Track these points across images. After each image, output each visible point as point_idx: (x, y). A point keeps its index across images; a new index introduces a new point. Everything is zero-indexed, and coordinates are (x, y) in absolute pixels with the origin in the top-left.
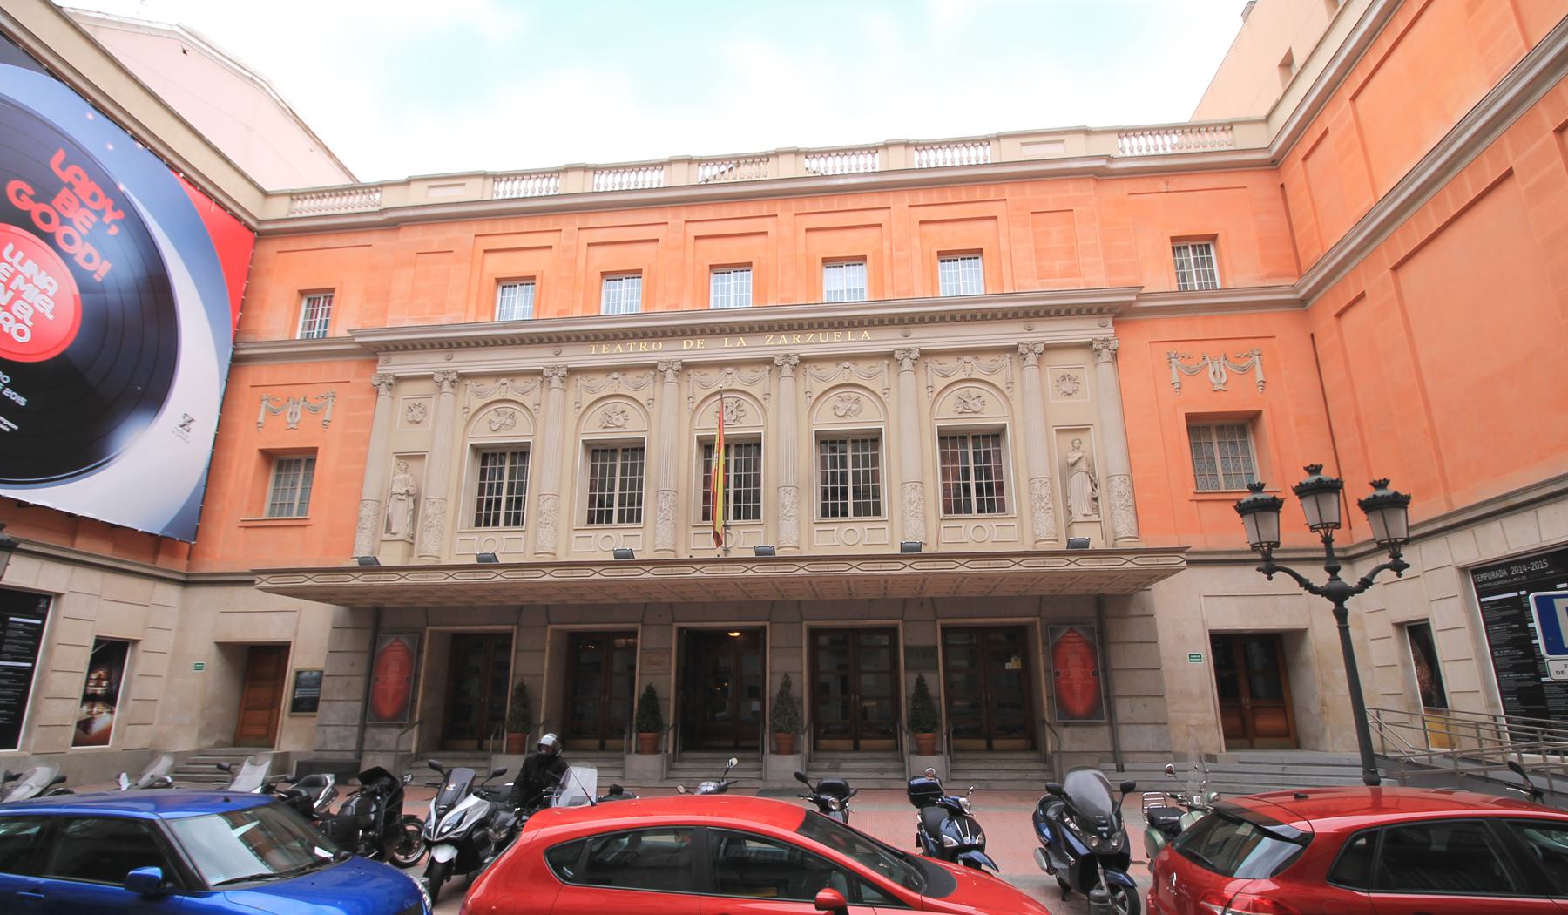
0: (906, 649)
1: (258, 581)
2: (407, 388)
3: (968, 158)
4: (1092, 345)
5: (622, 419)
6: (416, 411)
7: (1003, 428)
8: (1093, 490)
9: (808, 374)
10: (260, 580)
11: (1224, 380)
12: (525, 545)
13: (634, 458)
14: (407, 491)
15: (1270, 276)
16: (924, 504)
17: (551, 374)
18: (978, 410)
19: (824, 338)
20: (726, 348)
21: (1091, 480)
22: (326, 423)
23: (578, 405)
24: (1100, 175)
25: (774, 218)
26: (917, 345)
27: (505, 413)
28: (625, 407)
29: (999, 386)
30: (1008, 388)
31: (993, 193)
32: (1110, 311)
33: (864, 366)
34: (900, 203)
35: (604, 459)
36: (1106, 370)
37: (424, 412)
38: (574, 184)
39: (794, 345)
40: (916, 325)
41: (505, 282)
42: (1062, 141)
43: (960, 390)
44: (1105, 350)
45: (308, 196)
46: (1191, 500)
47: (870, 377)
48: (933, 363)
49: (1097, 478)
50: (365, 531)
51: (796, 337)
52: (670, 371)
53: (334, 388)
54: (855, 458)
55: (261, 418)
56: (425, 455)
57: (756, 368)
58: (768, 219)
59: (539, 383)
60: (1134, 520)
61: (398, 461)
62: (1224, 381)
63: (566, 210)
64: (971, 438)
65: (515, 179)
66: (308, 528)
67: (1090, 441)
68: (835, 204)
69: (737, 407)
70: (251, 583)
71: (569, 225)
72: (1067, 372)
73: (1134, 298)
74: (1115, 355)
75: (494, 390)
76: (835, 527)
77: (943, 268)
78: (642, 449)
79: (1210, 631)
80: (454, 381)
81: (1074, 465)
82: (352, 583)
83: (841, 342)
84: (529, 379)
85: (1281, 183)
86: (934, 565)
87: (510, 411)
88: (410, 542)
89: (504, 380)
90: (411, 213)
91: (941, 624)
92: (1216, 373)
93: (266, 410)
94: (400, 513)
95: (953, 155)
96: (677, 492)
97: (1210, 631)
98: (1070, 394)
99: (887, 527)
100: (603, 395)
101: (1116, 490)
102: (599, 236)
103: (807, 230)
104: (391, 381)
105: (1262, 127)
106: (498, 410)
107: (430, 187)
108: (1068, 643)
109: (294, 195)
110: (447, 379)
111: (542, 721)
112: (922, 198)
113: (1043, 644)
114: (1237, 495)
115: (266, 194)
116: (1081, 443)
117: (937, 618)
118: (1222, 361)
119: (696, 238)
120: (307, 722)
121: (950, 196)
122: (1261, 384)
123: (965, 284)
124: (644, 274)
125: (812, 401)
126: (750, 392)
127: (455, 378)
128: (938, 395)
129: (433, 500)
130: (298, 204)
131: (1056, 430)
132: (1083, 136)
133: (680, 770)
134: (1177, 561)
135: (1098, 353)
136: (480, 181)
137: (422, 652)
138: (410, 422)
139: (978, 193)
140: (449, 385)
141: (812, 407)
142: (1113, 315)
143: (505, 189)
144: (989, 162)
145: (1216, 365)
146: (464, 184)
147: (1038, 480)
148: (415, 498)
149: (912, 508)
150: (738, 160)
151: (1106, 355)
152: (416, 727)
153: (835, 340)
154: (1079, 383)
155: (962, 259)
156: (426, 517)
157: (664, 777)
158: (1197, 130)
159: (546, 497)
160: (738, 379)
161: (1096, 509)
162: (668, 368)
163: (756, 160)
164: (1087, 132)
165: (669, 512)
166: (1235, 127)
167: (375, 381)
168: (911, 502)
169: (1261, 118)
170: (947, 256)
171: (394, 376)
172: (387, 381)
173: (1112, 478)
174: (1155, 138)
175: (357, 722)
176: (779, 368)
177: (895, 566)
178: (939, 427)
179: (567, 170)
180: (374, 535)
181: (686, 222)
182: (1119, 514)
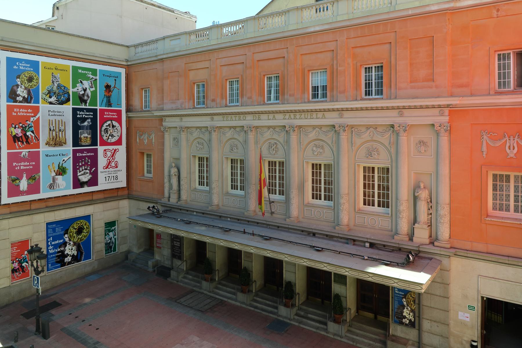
103: (301, 55)
119: (258, 61)
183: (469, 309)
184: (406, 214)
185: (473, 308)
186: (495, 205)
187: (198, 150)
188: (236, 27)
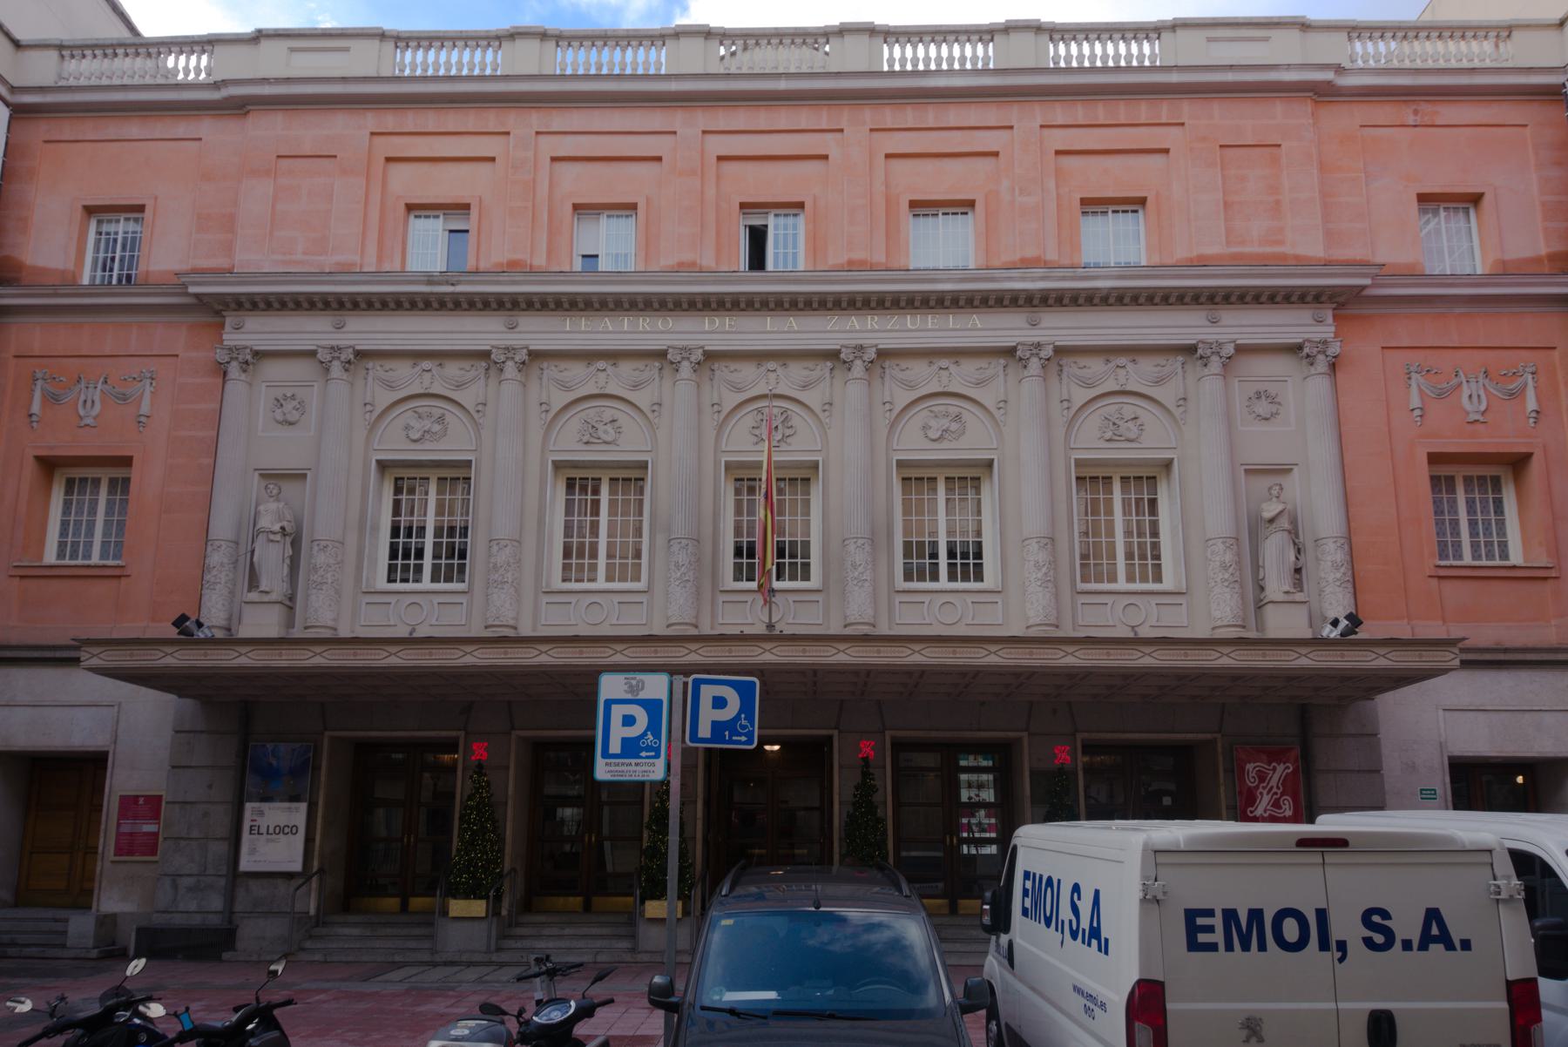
0: (1032, 773)
1: (83, 655)
2: (274, 370)
3: (572, 64)
4: (1196, 351)
5: (1135, 429)
6: (289, 406)
8: (1297, 558)
9: (887, 377)
10: (88, 656)
11: (1483, 408)
14: (283, 528)
16: (1055, 569)
17: (503, 358)
20: (728, 332)
21: (1295, 544)
22: (142, 419)
23: (544, 407)
24: (1322, 93)
25: (838, 135)
26: (702, 343)
27: (430, 415)
28: (618, 415)
30: (824, 411)
31: (1164, 111)
32: (1331, 298)
33: (969, 367)
34: (1027, 119)
35: (1139, 491)
36: (1317, 386)
37: (301, 407)
38: (525, 60)
39: (641, 332)
43: (1110, 407)
44: (1321, 357)
45: (88, 52)
47: (979, 383)
49: (1301, 540)
50: (218, 587)
52: (858, 362)
55: (36, 408)
56: (1291, 469)
57: (810, 364)
58: (829, 136)
59: (657, 371)
60: (1353, 601)
61: (263, 483)
64: (1461, 479)
65: (430, 46)
66: (123, 581)
67: (1293, 486)
68: (931, 116)
69: (782, 422)
70: (75, 661)
71: (524, 123)
72: (1261, 387)
73: (1368, 281)
74: (1333, 367)
75: (409, 377)
79: (1450, 758)
80: (349, 362)
81: (1271, 521)
82: (1297, 662)
84: (466, 364)
87: (437, 412)
88: (289, 603)
89: (426, 364)
91: (1083, 740)
92: (1472, 398)
93: (43, 396)
94: (272, 559)
96: (698, 541)
98: (1266, 419)
101: (1329, 558)
102: (568, 146)
103: (888, 156)
104: (249, 357)
106: (933, 409)
107: (292, 50)
109: (63, 49)
111: (315, 870)
112: (1059, 114)
113: (1226, 771)
114: (1541, 571)
115: (17, 44)
116: (1282, 489)
118: (1481, 380)
119: (720, 158)
121: (1101, 112)
122: (1534, 415)
124: (979, 206)
125: (1071, 415)
126: (456, 399)
127: (352, 357)
129: (503, 543)
130: (72, 66)
131: (1246, 470)
133: (522, 937)
134: (1451, 658)
136: (375, 44)
137: (319, 768)
138: (280, 423)
139: (1143, 111)
140: (340, 368)
141: (893, 425)
142: (1334, 306)
143: (412, 61)
146: (347, 50)
147: (1035, 540)
148: (294, 538)
151: (1321, 364)
152: (315, 879)
153: (583, 328)
154: (1279, 404)
156: (315, 569)
157: (493, 947)
158: (1461, 34)
159: (503, 543)
160: (788, 379)
161: (1298, 584)
162: (683, 358)
163: (469, 43)
164: (1304, 26)
165: (221, 572)
166: (1515, 34)
167: (221, 356)
168: (854, 566)
169: (1554, 22)
170: (1093, 205)
171: (251, 350)
172: (241, 357)
173: (1324, 541)
174: (1376, 44)
175: (224, 870)
176: (849, 366)
179: (514, 35)
180: (232, 593)
181: (704, 132)
183: (1422, 798)
184: (227, 575)
185: (1433, 792)
186: (1487, 533)
187: (415, 441)
188: (199, 59)
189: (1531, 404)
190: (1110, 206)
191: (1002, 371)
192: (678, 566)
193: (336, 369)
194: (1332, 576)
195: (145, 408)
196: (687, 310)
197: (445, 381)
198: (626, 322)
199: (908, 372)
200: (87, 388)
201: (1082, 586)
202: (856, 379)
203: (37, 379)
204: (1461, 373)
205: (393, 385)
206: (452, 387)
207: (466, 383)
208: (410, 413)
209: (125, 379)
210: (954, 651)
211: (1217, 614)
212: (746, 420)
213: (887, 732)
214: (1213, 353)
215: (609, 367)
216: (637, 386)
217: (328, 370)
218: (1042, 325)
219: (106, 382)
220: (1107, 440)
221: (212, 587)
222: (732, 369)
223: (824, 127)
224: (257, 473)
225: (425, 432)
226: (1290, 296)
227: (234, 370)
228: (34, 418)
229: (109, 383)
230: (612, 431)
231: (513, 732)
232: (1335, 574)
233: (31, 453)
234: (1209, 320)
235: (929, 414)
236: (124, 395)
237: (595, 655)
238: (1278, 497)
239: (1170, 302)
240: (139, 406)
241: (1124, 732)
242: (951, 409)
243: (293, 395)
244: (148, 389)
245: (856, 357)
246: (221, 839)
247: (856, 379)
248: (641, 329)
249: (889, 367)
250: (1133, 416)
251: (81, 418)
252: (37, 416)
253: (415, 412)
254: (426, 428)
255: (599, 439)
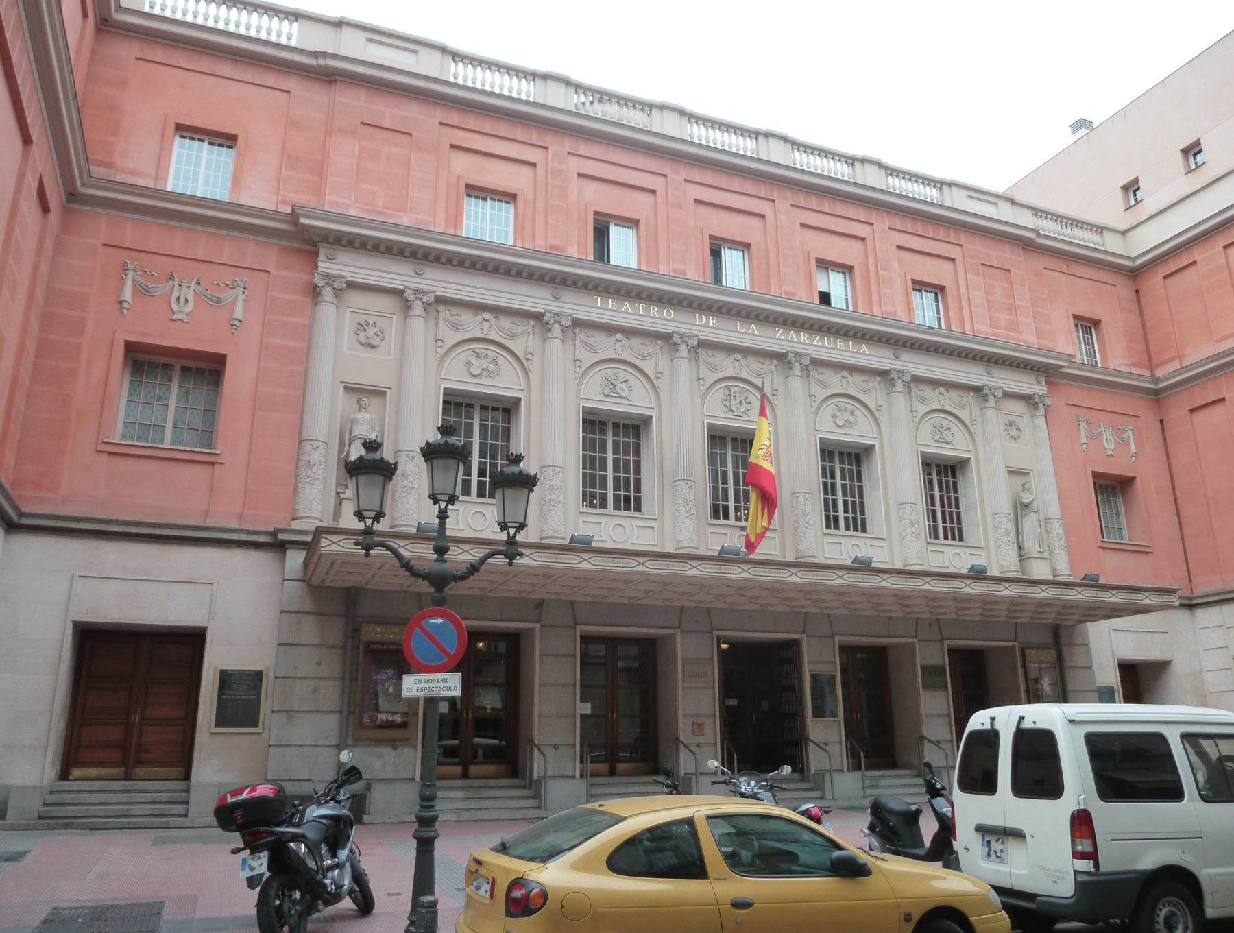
0: (923, 668)
2: (357, 299)
7: (647, 420)
12: (662, 532)
13: (744, 450)
15: (1135, 365)
18: (625, 395)
19: (701, 319)
20: (711, 327)
28: (629, 377)
29: (869, 406)
37: (381, 333)
40: (342, 248)
41: (919, 285)
42: (415, 52)
43: (610, 370)
46: (1099, 547)
47: (865, 391)
48: (581, 335)
50: (317, 482)
51: (804, 336)
53: (246, 277)
54: (616, 444)
55: (127, 294)
62: (1113, 448)
63: (275, 64)
69: (745, 399)
72: (1013, 418)
73: (1065, 364)
76: (603, 520)
77: (182, 147)
78: (751, 442)
79: (1118, 659)
83: (743, 333)
85: (1136, 289)
86: (556, 558)
90: (361, 69)
93: (134, 286)
95: (207, 10)
97: (1118, 659)
99: (885, 545)
100: (466, 338)
102: (591, 168)
105: (1119, 237)
106: (838, 404)
108: (1049, 662)
110: (332, 285)
117: (576, 624)
118: (193, 286)
120: (240, 739)
123: (476, 227)
128: (709, 387)
131: (1008, 470)
132: (563, 85)
135: (674, 347)
138: (361, 344)
144: (531, 99)
145: (184, 289)
147: (551, 468)
149: (914, 529)
150: (603, 96)
155: (492, 199)
166: (1105, 232)
169: (1119, 230)
177: (829, 576)
178: (445, 388)
182: (1058, 554)
189: (1133, 449)
190: (489, 195)
191: (531, 330)
192: (686, 502)
193: (418, 308)
194: (910, 530)
195: (239, 313)
196: (548, 282)
197: (501, 331)
198: (827, 342)
199: (822, 376)
200: (180, 286)
201: (826, 531)
202: (796, 376)
203: (128, 269)
204: (1102, 425)
205: (716, 368)
206: (507, 337)
207: (518, 335)
208: (470, 352)
209: (218, 284)
210: (667, 564)
211: (1005, 563)
212: (719, 394)
213: (578, 626)
214: (796, 360)
215: (493, 319)
216: (645, 357)
217: (410, 307)
218: (424, 276)
219: (199, 284)
220: (936, 441)
221: (312, 482)
222: (920, 389)
223: (762, 196)
224: (343, 385)
225: (483, 369)
226: (777, 319)
227: (327, 293)
228: (125, 305)
229: (202, 284)
230: (626, 389)
231: (578, 626)
232: (551, 495)
233: (122, 337)
234: (554, 296)
235: (835, 407)
236: (218, 298)
237: (624, 565)
238: (1028, 490)
239: (621, 293)
240: (232, 311)
241: (502, 620)
242: (489, 353)
243: (374, 323)
244: (241, 297)
245: (417, 298)
246: (332, 712)
247: (796, 376)
248: (651, 315)
249: (443, 311)
250: (625, 379)
251: (173, 312)
252: (129, 303)
253: (474, 352)
254: (484, 367)
255: (616, 393)
